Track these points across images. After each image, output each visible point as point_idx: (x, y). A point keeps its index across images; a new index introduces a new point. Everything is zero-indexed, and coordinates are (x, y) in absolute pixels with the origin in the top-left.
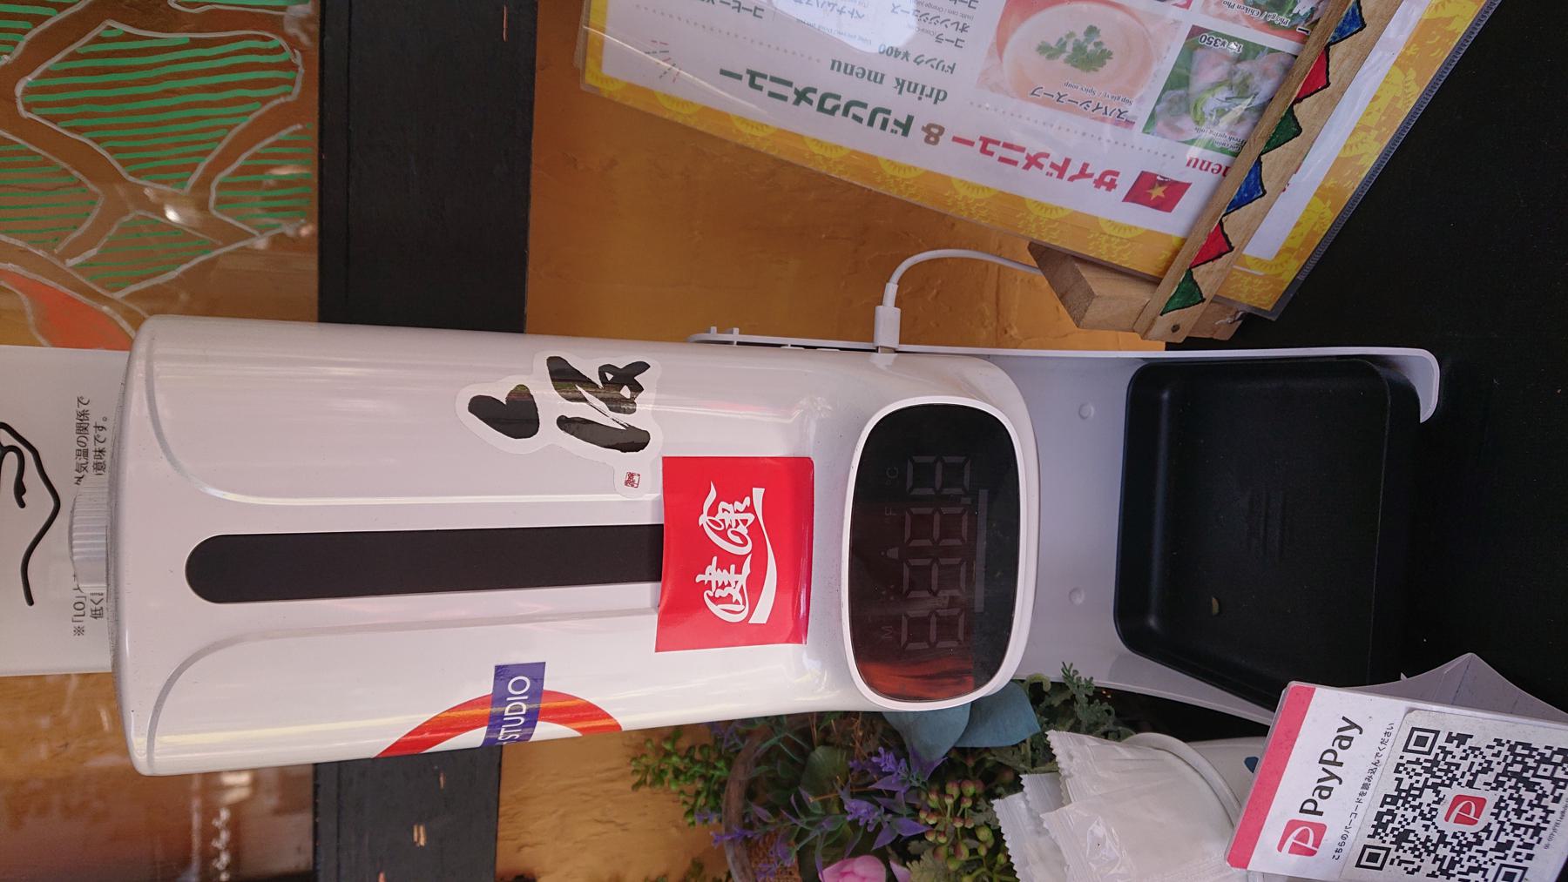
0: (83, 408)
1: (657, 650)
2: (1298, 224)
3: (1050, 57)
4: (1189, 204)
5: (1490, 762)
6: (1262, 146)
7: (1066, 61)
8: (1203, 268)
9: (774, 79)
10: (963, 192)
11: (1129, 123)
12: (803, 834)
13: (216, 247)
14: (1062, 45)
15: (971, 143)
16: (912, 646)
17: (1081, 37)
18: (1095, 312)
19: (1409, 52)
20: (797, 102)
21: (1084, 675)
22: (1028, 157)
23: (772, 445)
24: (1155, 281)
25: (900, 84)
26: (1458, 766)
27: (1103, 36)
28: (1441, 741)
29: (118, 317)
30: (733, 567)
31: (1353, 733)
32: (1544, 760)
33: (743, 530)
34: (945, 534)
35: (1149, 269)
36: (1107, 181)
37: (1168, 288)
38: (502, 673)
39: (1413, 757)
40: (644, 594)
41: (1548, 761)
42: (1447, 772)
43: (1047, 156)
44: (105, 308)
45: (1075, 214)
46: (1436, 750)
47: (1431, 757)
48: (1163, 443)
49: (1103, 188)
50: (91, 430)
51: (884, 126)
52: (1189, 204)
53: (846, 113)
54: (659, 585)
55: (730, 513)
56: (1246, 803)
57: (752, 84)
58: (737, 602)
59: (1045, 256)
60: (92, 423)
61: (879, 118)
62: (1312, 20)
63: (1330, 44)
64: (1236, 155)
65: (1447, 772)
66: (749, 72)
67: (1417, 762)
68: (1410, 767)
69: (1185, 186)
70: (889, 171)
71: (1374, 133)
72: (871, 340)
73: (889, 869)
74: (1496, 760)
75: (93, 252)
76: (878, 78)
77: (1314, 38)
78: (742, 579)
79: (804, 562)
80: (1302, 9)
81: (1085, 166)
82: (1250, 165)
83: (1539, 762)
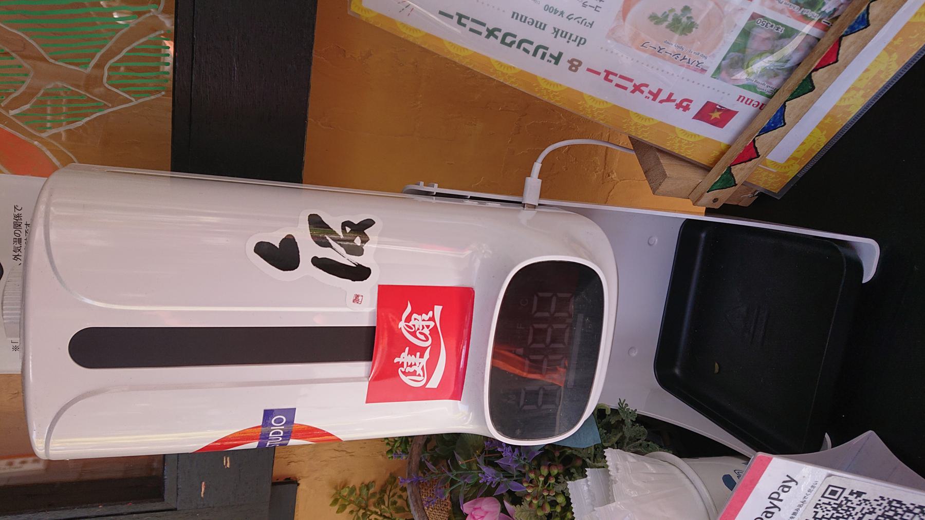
0: (17, 212)
1: (367, 402)
2: (803, 143)
3: (656, 23)
4: (734, 125)
5: (874, 509)
6: (788, 96)
7: (667, 27)
8: (739, 166)
9: (473, 20)
10: (590, 103)
11: (703, 71)
12: (453, 482)
13: (107, 107)
14: (666, 16)
15: (599, 74)
16: (526, 407)
17: (679, 12)
18: (666, 186)
19: (896, 43)
20: (488, 37)
21: (631, 408)
22: (635, 85)
23: (449, 279)
24: (707, 169)
25: (556, 31)
26: (854, 509)
27: (693, 14)
28: (846, 494)
29: (44, 149)
30: (418, 354)
31: (792, 484)
32: (909, 511)
33: (427, 331)
34: (553, 341)
35: (704, 161)
36: (684, 105)
37: (715, 175)
38: (268, 414)
39: (827, 501)
40: (360, 369)
41: (911, 511)
42: (846, 511)
43: (647, 86)
44: (36, 143)
45: (661, 124)
46: (842, 498)
47: (838, 502)
48: (701, 249)
49: (681, 109)
50: (23, 226)
51: (543, 57)
52: (734, 125)
53: (519, 47)
54: (369, 363)
55: (419, 321)
56: (721, 514)
57: (459, 22)
58: (419, 375)
59: (639, 146)
60: (24, 222)
61: (541, 51)
62: (834, 17)
63: (843, 36)
64: (770, 97)
65: (846, 511)
66: (458, 14)
67: (829, 504)
68: (824, 506)
69: (733, 113)
70: (544, 85)
71: (862, 92)
72: (521, 194)
73: (503, 504)
74: (879, 508)
75: (27, 107)
76: (542, 26)
77: (832, 30)
78: (423, 361)
79: (465, 331)
80: (828, 8)
81: (671, 95)
82: (779, 106)
83: (905, 512)
